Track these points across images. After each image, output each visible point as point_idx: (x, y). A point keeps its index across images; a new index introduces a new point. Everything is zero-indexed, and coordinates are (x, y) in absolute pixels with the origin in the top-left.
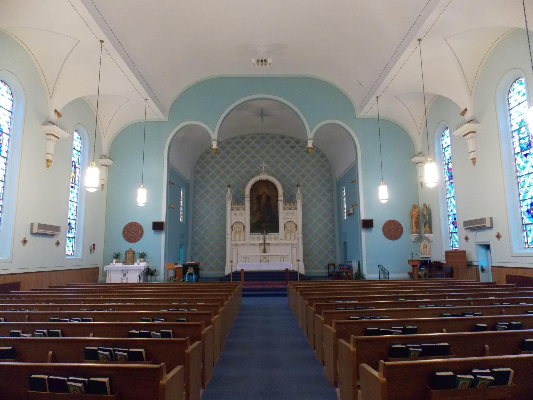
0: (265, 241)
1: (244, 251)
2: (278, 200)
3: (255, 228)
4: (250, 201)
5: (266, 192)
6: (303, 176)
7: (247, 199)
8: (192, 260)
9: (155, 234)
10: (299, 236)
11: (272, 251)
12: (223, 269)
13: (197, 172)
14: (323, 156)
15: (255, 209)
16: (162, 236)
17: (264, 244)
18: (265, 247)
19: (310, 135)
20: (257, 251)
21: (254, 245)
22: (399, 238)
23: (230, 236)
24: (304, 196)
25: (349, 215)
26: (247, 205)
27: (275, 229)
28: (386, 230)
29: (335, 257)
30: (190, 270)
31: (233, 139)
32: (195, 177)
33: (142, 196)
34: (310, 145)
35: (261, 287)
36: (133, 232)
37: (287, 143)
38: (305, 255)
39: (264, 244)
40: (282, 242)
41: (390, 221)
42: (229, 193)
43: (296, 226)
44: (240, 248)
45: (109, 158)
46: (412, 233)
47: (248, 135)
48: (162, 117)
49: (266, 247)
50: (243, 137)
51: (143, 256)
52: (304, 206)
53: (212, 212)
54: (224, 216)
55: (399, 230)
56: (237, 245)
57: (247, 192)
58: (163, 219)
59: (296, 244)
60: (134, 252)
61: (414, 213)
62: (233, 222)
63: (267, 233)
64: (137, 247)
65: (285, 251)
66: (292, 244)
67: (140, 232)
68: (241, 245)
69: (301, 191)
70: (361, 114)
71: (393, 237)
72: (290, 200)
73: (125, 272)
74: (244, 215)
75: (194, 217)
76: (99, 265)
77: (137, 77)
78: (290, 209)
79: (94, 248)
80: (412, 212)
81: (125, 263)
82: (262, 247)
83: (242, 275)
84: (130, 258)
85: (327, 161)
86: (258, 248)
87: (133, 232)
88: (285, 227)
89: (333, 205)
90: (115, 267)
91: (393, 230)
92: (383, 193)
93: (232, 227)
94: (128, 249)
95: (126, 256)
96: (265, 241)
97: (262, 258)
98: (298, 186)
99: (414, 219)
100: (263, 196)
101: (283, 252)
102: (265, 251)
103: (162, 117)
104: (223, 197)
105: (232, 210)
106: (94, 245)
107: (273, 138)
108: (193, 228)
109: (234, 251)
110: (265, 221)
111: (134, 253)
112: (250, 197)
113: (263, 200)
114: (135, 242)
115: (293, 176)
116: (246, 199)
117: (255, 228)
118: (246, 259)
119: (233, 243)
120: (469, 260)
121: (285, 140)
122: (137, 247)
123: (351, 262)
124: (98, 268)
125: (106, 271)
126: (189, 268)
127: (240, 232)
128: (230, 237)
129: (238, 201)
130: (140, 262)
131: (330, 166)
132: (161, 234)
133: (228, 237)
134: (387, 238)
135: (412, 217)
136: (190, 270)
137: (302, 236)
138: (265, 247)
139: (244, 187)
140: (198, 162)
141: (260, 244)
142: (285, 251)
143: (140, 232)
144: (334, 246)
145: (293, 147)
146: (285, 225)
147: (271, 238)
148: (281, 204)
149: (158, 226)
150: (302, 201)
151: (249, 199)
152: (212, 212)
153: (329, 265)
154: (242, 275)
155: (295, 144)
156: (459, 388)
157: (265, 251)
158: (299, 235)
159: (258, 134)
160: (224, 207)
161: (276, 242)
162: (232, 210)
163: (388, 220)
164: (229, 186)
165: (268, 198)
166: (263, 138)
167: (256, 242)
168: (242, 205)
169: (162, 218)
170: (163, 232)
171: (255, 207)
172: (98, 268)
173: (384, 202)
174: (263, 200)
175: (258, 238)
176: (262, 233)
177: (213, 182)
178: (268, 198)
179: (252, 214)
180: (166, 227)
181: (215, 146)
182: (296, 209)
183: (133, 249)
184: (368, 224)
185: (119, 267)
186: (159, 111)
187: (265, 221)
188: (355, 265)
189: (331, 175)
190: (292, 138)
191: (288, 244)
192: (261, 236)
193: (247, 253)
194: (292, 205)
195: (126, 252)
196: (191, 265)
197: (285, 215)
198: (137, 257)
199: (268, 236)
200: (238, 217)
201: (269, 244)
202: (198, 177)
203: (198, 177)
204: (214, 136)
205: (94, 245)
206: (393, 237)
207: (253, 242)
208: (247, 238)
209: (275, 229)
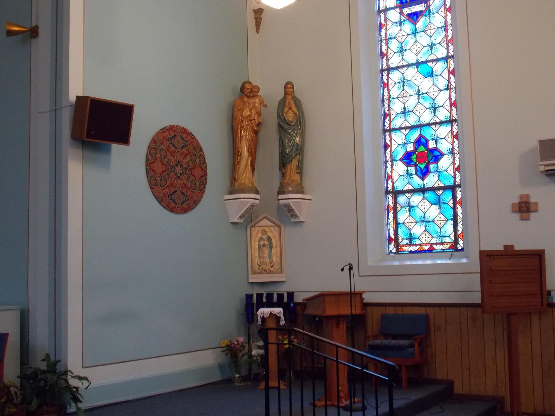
91: (179, 170)
180: (47, 128)
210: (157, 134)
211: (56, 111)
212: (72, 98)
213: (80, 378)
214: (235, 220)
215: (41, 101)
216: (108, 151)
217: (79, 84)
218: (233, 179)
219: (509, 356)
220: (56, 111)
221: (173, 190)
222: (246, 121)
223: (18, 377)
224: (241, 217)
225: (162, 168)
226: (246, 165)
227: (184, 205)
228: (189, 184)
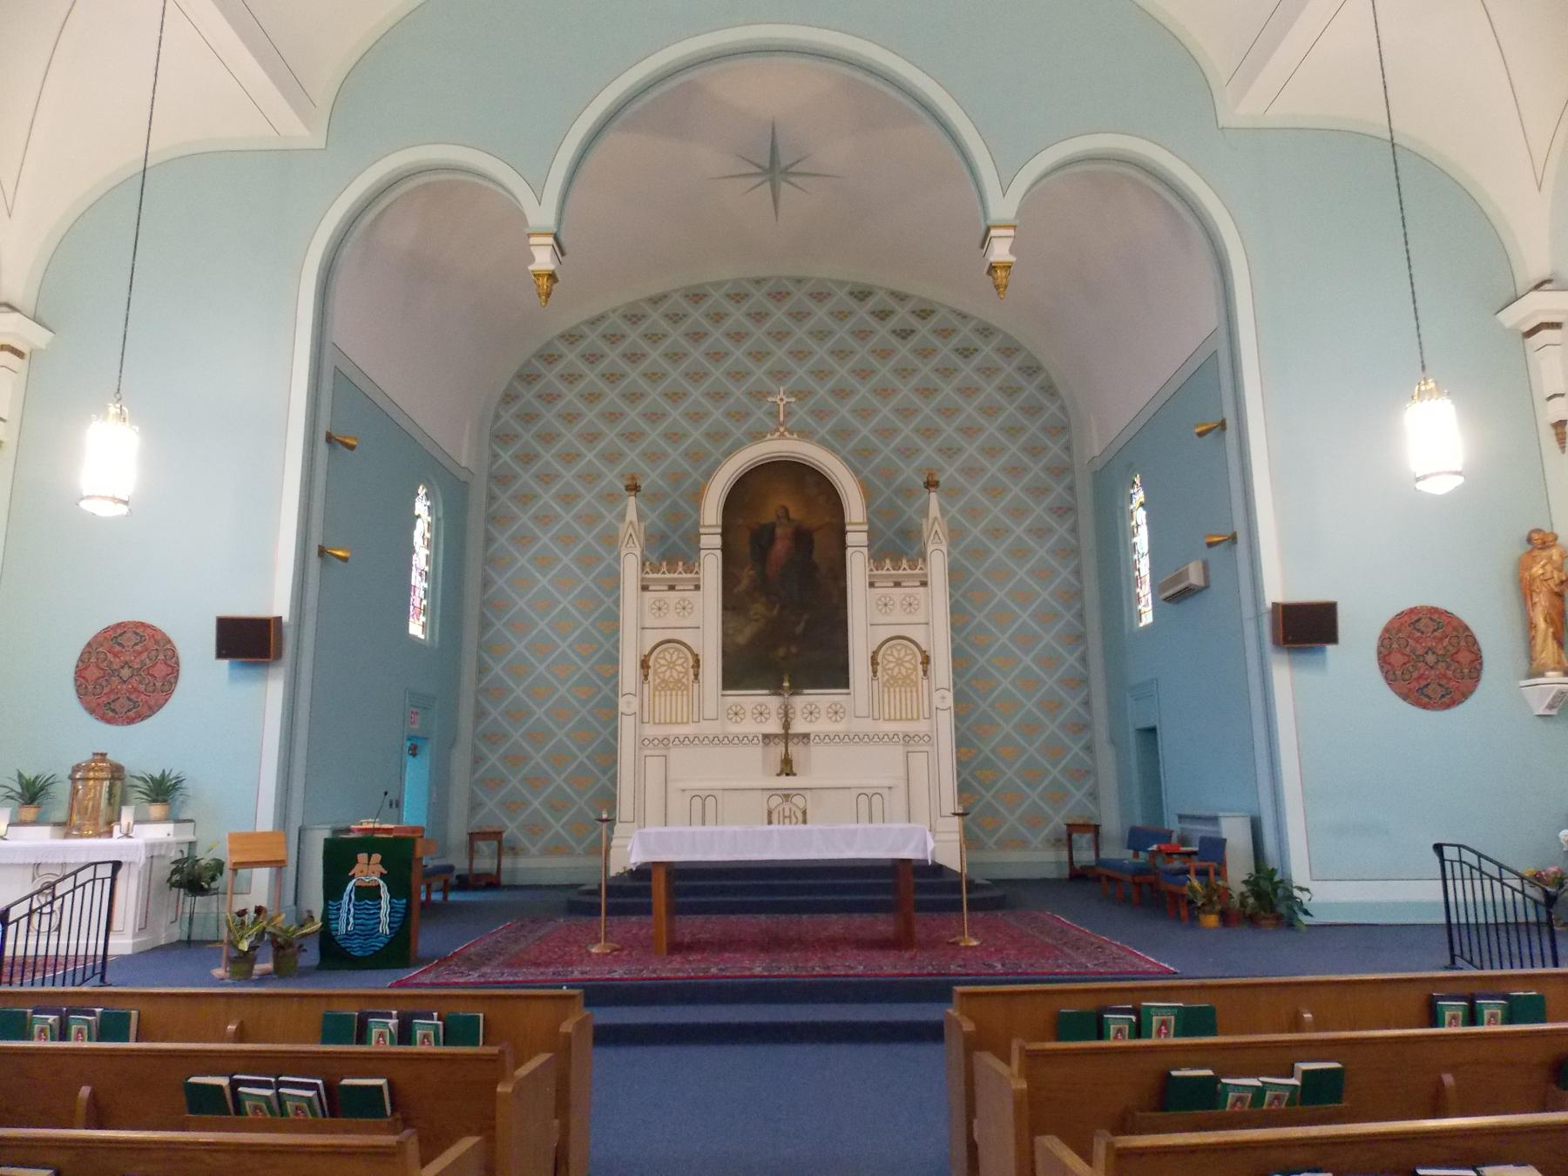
0: (786, 726)
1: (697, 770)
2: (843, 546)
3: (742, 669)
4: (726, 549)
5: (792, 515)
6: (950, 452)
7: (712, 541)
8: (787, 806)
10: (937, 702)
11: (817, 768)
12: (602, 849)
13: (502, 438)
14: (1031, 369)
15: (744, 584)
17: (786, 737)
18: (786, 749)
19: (1003, 206)
20: (753, 769)
21: (743, 740)
22: (1465, 696)
23: (635, 702)
24: (955, 535)
25: (1176, 595)
26: (711, 566)
27: (835, 674)
28: (1397, 659)
29: (1093, 795)
30: (368, 871)
31: (655, 301)
32: (495, 456)
33: (108, 462)
34: (1000, 251)
35: (758, 967)
36: (125, 673)
37: (883, 315)
38: (963, 788)
39: (786, 737)
40: (867, 726)
41: (1412, 611)
42: (631, 515)
43: (926, 660)
44: (675, 754)
45: (35, 319)
46: (1533, 674)
47: (718, 285)
48: (299, 132)
49: (792, 749)
50: (696, 296)
51: (162, 791)
52: (956, 575)
53: (564, 603)
54: (611, 622)
55: (1464, 657)
56: (665, 742)
57: (711, 512)
58: (279, 605)
59: (929, 738)
61: (1537, 570)
62: (652, 638)
63: (796, 689)
64: (140, 747)
65: (877, 768)
66: (907, 738)
67: (160, 670)
68: (686, 741)
69: (943, 511)
70: (1246, 107)
71: (1434, 690)
72: (897, 546)
74: (698, 613)
75: (485, 625)
77: (262, 62)
78: (897, 585)
80: (1523, 565)
81: (66, 828)
82: (778, 750)
83: (659, 886)
84: (111, 790)
85: (1050, 390)
86: (756, 752)
87: (126, 673)
88: (874, 662)
89: (1077, 572)
90: (13, 850)
91: (1431, 658)
92: (1435, 441)
93: (644, 664)
94: (84, 757)
95: (75, 792)
96: (786, 726)
97: (776, 801)
98: (931, 484)
99: (1542, 601)
100: (779, 531)
101: (869, 778)
102: (787, 767)
103: (299, 132)
104: (610, 540)
105: (645, 588)
107: (820, 296)
108: (482, 670)
109: (654, 766)
110: (788, 623)
111: (117, 772)
112: (724, 535)
113: (781, 547)
114: (131, 721)
115: (907, 452)
116: (705, 541)
117: (742, 669)
118: (704, 805)
119: (650, 731)
121: (870, 304)
122: (140, 747)
123: (1214, 820)
126: (363, 857)
127: (679, 685)
128: (635, 706)
129: (670, 551)
131: (1063, 408)
132: (266, 678)
133: (627, 705)
134: (1405, 697)
135: (1526, 590)
136: (368, 871)
137: (950, 701)
138: (786, 749)
139: (697, 496)
140: (509, 398)
141: (766, 736)
142: (877, 768)
144: (1089, 748)
145: (905, 334)
146: (875, 653)
147: (814, 709)
148: (857, 564)
149: (246, 641)
150: (949, 553)
151: (717, 541)
152: (564, 603)
153: (1072, 828)
154: (659, 886)
155: (914, 322)
156: (1265, 1107)
157: (787, 767)
158: (936, 696)
159: (758, 282)
160: (612, 581)
161: (839, 727)
162: (645, 588)
163: (1412, 605)
164: (634, 488)
165: (803, 538)
166: (779, 296)
167: (750, 727)
168: (689, 570)
169: (274, 598)
170: (272, 671)
171: (747, 576)
173: (1442, 486)
174: (781, 547)
175: (758, 710)
176: (777, 689)
177: (568, 476)
178: (803, 538)
179: (732, 604)
180: (300, 647)
181: (543, 259)
182: (924, 584)
184: (1307, 627)
185: (25, 850)
186: (254, 63)
187: (788, 623)
188: (1235, 834)
189: (1067, 448)
190: (902, 298)
191: (890, 738)
192: (773, 702)
193: (706, 781)
194: (905, 569)
195: (76, 769)
196: (369, 843)
197: (872, 610)
199: (800, 702)
200: (672, 619)
201: (806, 736)
202: (506, 457)
203: (506, 457)
204: (542, 214)
206: (1434, 690)
207: (734, 729)
208: (710, 709)
209: (835, 674)
210: (1391, 622)
211: (1258, 617)
212: (1269, 605)
213: (1301, 889)
214: (1541, 712)
215: (1247, 610)
216: (1323, 651)
217: (1278, 588)
218: (1531, 659)
219: (804, 1025)
220: (1258, 617)
221: (1423, 683)
222: (1538, 583)
223: (1245, 882)
224: (1551, 707)
225: (98, 673)
226: (1545, 640)
227: (131, 714)
228: (1450, 673)
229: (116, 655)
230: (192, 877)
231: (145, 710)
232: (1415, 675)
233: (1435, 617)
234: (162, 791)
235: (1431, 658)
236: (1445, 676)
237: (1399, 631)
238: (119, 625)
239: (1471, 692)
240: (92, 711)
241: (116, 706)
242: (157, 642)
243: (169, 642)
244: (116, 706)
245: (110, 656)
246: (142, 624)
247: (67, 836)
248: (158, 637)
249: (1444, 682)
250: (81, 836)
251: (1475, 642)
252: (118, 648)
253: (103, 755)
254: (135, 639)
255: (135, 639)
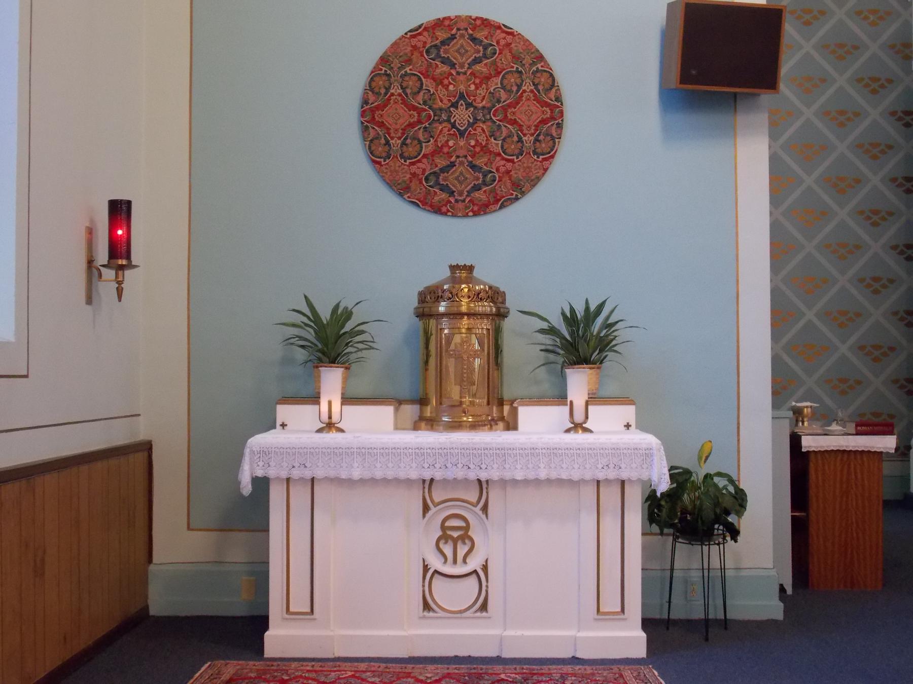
9: (668, 132)
16: (745, 160)
28: (396, 116)
51: (583, 341)
60: (495, 295)
71: (460, 178)
73: (455, 512)
76: (160, 416)
79: (120, 252)
81: (425, 404)
87: (462, 116)
94: (439, 274)
106: (120, 211)
114: (482, 209)
120: (644, 446)
124: (146, 448)
125: (262, 485)
130: (594, 399)
132: (731, 132)
143: (528, 113)
170: (742, 119)
172: (146, 448)
183: (488, 274)
195: (429, 297)
198: (522, 347)
205: (120, 211)
221: (441, 162)
229: (439, 81)
230: (689, 512)
231: (504, 189)
232: (427, 148)
233: (481, 35)
234: (583, 341)
235: (462, 116)
236: (485, 149)
237: (409, 61)
238: (439, 23)
239: (534, 182)
240: (402, 190)
241: (450, 179)
242: (516, 58)
243: (540, 58)
244: (450, 179)
245: (428, 83)
246: (486, 23)
247: (431, 423)
248: (517, 47)
249: (480, 162)
250: (456, 426)
251: (553, 83)
252: (443, 69)
253: (470, 269)
254: (473, 51)
255: (473, 51)
